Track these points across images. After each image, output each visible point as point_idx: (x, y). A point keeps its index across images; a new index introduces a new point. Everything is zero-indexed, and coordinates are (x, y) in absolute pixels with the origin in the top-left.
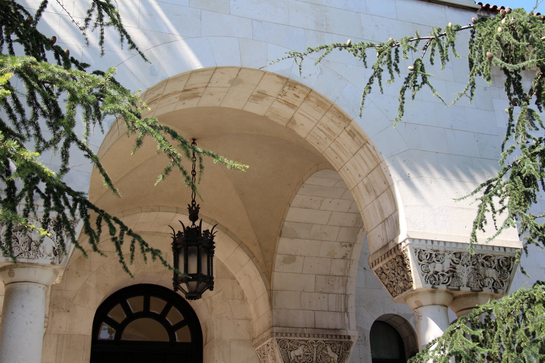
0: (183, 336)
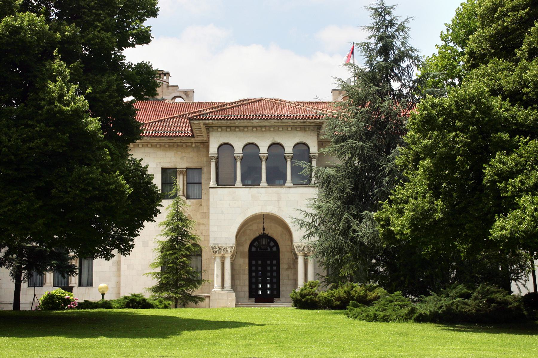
0: (275, 249)
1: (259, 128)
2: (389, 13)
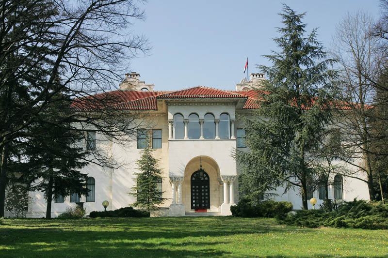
0: (206, 179)
1: (199, 104)
2: (298, 20)
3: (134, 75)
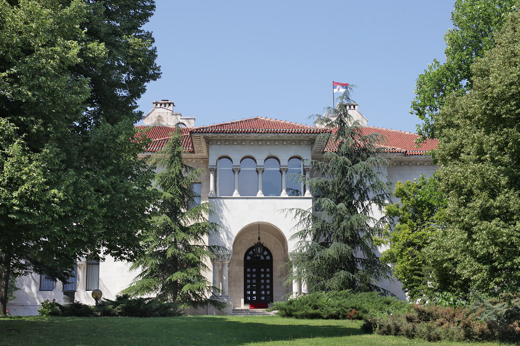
0: (268, 258)
3: (165, 104)
